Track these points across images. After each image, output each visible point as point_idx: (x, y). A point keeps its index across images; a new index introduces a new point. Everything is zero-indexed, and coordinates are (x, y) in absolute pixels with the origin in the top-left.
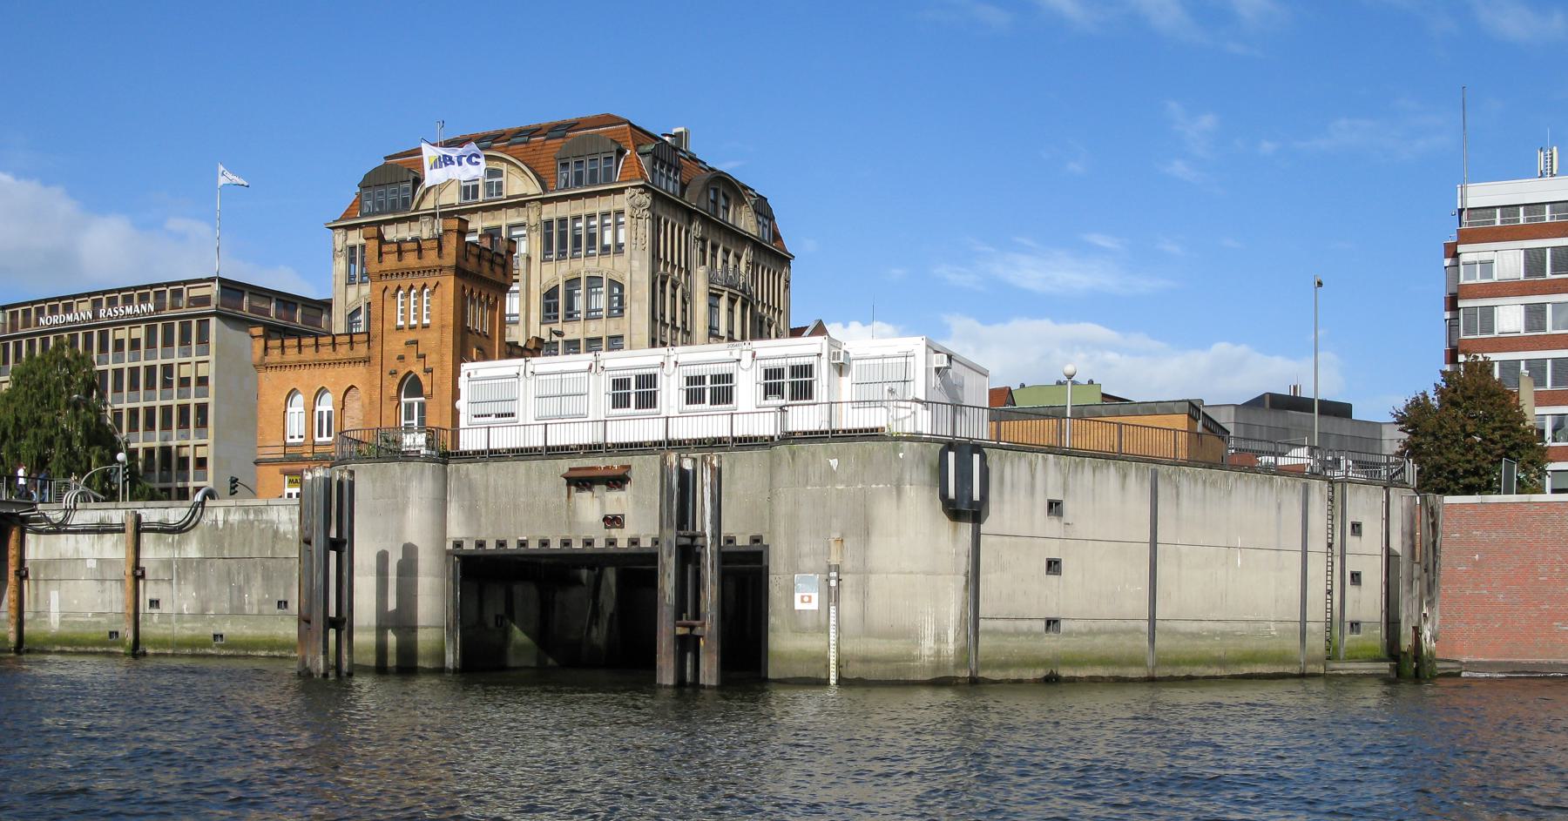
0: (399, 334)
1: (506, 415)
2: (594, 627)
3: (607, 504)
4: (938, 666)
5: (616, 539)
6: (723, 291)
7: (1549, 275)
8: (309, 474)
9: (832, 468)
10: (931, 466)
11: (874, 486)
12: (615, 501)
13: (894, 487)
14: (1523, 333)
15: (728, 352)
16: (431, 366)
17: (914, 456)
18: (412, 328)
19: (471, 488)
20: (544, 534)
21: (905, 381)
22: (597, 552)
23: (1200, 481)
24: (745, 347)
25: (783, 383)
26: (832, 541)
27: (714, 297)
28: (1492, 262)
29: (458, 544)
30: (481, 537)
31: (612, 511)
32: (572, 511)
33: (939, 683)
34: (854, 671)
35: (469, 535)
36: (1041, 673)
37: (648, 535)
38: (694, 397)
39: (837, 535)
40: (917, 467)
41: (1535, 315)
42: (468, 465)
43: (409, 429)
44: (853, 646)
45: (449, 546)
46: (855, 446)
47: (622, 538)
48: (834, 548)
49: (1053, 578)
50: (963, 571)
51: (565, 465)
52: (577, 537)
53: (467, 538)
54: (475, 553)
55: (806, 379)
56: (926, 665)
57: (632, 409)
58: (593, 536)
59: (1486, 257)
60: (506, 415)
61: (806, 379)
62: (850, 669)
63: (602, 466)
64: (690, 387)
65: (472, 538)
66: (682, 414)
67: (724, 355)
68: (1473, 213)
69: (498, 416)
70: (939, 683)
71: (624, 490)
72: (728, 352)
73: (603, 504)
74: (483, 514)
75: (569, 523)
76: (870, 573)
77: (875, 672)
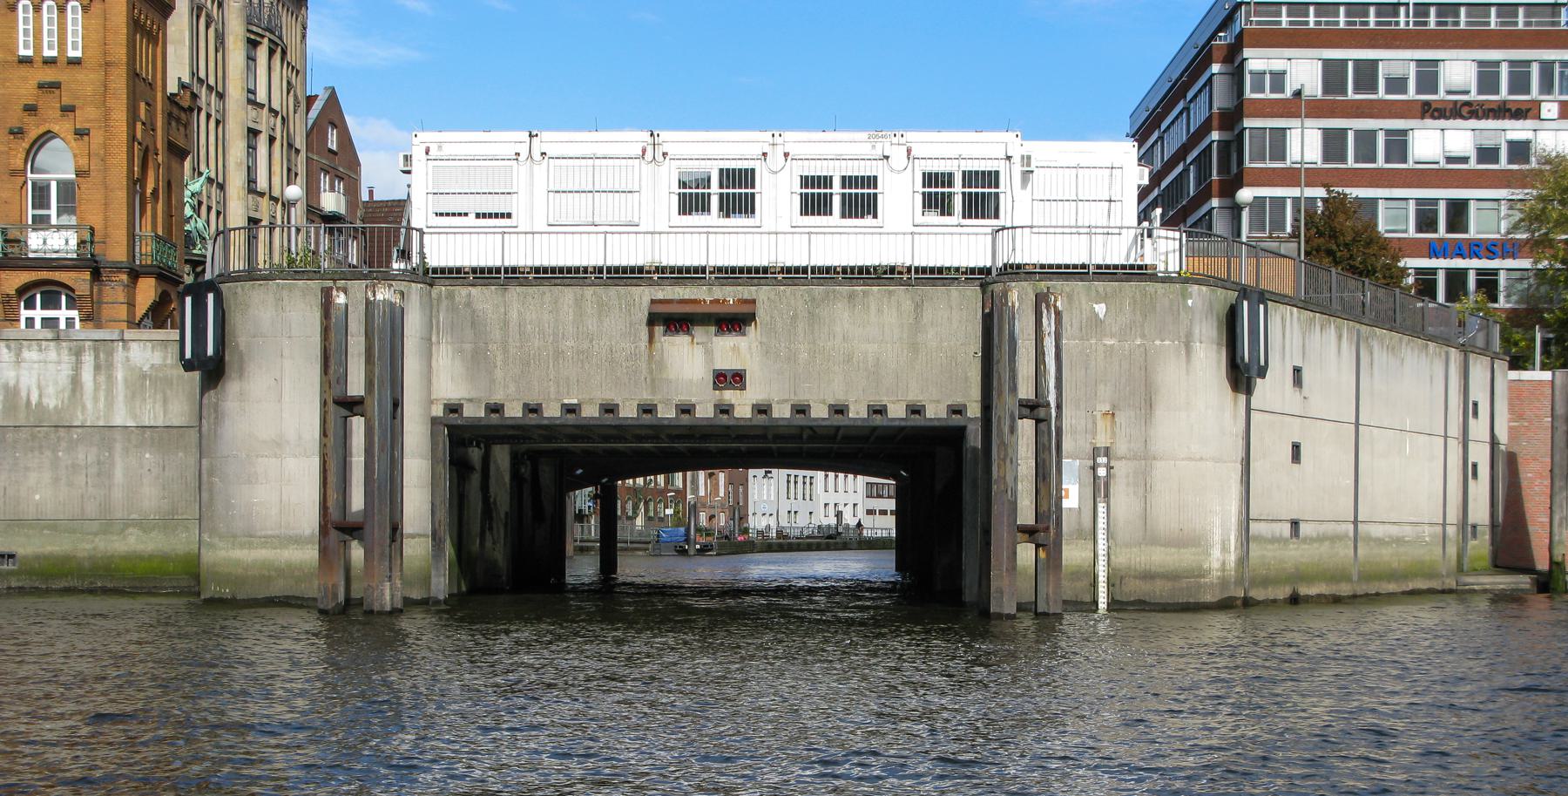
0: (24, 71)
1: (503, 216)
2: (488, 533)
3: (717, 355)
4: (1224, 582)
5: (732, 406)
6: (262, 37)
7: (1351, 94)
8: (342, 295)
9: (1097, 315)
10: (1218, 318)
11: (1158, 342)
12: (729, 350)
13: (1182, 345)
14: (1320, 165)
15: (869, 145)
16: (87, 125)
17: (1203, 305)
18: (50, 62)
19: (475, 322)
20: (837, 394)
21: (1110, 201)
22: (700, 423)
23: (1385, 348)
24: (895, 140)
25: (831, 194)
26: (1099, 416)
27: (253, 44)
28: (1284, 73)
29: (453, 409)
30: (497, 398)
31: (726, 363)
32: (656, 364)
33: (1225, 605)
34: (1135, 589)
35: (473, 395)
36: (1283, 592)
37: (786, 401)
38: (814, 204)
39: (1106, 407)
40: (1201, 322)
41: (1333, 143)
42: (470, 288)
43: (41, 222)
44: (1127, 558)
45: (438, 411)
46: (1131, 286)
47: (742, 405)
48: (1102, 424)
49: (1296, 466)
50: (1240, 459)
51: (643, 296)
52: (667, 402)
53: (470, 400)
54: (713, 423)
55: (819, 191)
56: (1215, 581)
57: (835, 218)
58: (694, 400)
59: (1277, 65)
60: (503, 216)
61: (869, 191)
62: (1126, 589)
63: (708, 299)
64: (927, 190)
65: (479, 401)
66: (674, 230)
67: (865, 149)
68: (1260, 8)
69: (478, 216)
70: (1225, 605)
71: (745, 335)
72: (869, 145)
73: (709, 353)
74: (499, 363)
75: (653, 380)
76: (1155, 458)
77: (1159, 591)
